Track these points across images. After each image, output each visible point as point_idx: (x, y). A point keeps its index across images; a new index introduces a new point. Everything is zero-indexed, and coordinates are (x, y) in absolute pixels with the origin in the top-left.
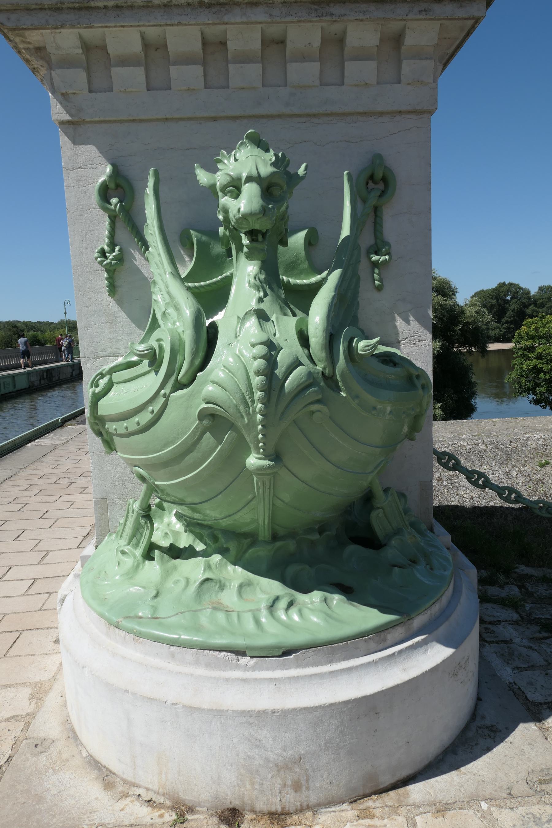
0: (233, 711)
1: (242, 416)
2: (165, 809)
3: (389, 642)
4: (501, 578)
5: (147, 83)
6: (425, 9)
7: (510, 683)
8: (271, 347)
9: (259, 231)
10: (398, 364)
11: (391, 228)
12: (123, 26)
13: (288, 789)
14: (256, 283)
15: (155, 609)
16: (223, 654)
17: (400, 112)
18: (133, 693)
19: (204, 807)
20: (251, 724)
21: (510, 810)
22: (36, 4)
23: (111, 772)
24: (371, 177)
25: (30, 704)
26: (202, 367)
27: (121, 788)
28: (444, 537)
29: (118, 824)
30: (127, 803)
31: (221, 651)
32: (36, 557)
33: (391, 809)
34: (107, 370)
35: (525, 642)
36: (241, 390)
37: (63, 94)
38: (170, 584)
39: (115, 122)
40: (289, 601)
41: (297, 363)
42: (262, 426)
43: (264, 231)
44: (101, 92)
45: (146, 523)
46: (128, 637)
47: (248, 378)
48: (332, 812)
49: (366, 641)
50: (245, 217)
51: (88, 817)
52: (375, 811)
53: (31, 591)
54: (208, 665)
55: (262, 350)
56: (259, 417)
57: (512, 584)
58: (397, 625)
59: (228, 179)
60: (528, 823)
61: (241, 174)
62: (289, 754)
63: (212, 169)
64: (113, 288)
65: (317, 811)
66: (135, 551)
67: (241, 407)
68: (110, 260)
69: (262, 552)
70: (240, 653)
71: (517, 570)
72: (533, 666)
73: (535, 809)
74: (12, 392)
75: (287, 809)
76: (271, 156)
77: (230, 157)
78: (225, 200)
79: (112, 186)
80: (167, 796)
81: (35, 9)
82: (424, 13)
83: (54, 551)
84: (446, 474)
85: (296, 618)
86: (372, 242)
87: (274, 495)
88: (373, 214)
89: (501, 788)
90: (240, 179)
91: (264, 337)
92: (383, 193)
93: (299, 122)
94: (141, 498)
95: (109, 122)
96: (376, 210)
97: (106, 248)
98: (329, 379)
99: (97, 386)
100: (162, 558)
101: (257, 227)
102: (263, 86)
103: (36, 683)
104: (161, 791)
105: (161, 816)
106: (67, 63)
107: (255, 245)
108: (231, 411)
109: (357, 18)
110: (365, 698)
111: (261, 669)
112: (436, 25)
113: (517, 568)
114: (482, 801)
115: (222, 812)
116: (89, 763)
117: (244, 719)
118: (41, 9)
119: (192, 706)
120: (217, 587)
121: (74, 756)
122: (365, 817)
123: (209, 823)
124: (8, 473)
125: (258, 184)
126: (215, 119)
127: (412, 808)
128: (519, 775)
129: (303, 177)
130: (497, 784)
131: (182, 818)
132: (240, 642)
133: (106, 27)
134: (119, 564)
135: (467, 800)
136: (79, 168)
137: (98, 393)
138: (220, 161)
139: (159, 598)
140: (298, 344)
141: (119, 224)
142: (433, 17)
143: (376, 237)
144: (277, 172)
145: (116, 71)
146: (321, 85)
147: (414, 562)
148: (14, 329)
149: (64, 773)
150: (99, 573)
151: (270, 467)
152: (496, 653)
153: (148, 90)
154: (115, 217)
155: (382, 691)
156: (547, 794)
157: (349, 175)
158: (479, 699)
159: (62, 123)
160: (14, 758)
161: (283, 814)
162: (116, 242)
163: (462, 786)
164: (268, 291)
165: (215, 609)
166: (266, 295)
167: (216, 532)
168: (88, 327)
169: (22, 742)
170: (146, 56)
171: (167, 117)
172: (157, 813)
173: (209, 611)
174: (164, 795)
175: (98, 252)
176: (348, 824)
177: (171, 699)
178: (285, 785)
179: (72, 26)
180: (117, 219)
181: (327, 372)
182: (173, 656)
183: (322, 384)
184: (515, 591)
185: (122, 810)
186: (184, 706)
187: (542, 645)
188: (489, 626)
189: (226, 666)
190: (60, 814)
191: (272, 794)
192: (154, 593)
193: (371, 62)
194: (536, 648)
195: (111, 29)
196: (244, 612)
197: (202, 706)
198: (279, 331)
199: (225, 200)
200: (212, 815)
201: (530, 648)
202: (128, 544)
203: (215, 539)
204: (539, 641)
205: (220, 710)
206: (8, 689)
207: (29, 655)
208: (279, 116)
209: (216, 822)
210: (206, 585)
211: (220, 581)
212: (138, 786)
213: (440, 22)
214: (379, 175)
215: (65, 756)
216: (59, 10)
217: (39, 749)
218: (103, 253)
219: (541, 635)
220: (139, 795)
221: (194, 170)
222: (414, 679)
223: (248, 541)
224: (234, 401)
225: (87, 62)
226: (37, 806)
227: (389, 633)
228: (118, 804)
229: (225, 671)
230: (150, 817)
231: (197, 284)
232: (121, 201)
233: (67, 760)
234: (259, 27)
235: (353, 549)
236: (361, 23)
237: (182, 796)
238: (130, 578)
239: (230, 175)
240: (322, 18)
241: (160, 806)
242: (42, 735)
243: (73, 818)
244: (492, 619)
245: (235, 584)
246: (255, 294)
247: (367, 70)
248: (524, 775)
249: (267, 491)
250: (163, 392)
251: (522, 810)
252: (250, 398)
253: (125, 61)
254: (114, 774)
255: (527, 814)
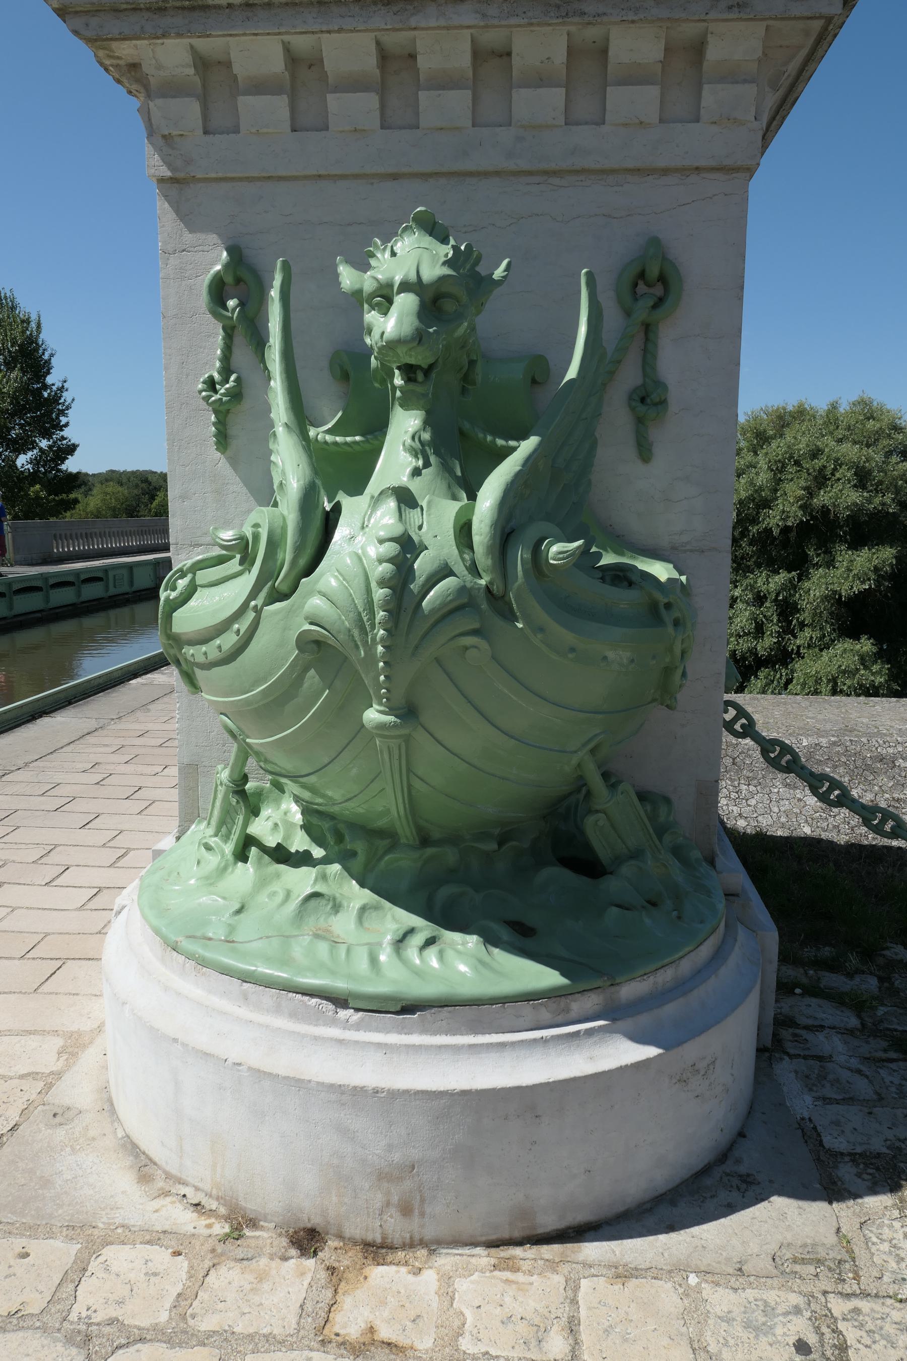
0: (318, 1083)
1: (357, 647)
2: (216, 1219)
3: (573, 1015)
4: (853, 960)
5: (293, 118)
6: (738, 4)
7: (803, 1119)
8: (407, 547)
9: (418, 367)
10: (635, 584)
11: (671, 362)
12: (256, 35)
13: (392, 1210)
14: (413, 444)
15: (232, 929)
16: (314, 1001)
17: (697, 168)
18: (184, 1045)
19: (271, 1222)
20: (343, 1104)
21: (731, 1291)
22: (127, 3)
23: (151, 1160)
24: (642, 275)
25: (58, 1060)
26: (309, 570)
27: (160, 1184)
28: (736, 875)
29: (146, 1228)
30: (165, 1203)
31: (312, 995)
32: (110, 856)
33: (547, 1263)
34: (188, 565)
35: (854, 1063)
36: (356, 607)
37: (164, 137)
38: (263, 898)
39: (240, 179)
40: (429, 936)
41: (445, 571)
42: (384, 663)
43: (425, 366)
44: (222, 133)
45: (238, 802)
46: (187, 965)
47: (369, 591)
48: (457, 1254)
49: (534, 1007)
50: (392, 345)
51: (107, 1214)
52: (522, 1262)
53: (91, 905)
54: (293, 1015)
55: (391, 549)
56: (380, 649)
57: (871, 973)
58: (591, 990)
59: (375, 284)
60: (754, 1312)
61: (393, 278)
62: (397, 1157)
63: (363, 265)
64: (223, 439)
65: (434, 1250)
66: (224, 847)
67: (356, 633)
68: (221, 394)
69: (405, 861)
70: (340, 1001)
71: (887, 953)
72: (851, 1099)
73: (772, 1296)
74: (127, 594)
75: (390, 1241)
76: (447, 251)
77: (384, 249)
78: (371, 317)
79: (229, 280)
80: (222, 1201)
81: (126, 10)
82: (736, 9)
83: (137, 849)
84: (887, 796)
85: (434, 963)
86: (639, 381)
87: (409, 770)
88: (642, 334)
89: (728, 1260)
90: (390, 285)
91: (398, 530)
92: (659, 302)
93: (527, 184)
94: (230, 764)
95: (232, 179)
96: (648, 329)
97: (216, 376)
98: (497, 600)
99: (174, 589)
100: (260, 860)
101: (412, 361)
102: (473, 126)
103: (72, 1033)
104: (214, 1192)
105: (209, 1226)
106: (172, 89)
107: (412, 386)
108: (341, 637)
109: (624, 18)
110: (519, 1089)
111: (369, 1029)
112: (760, 29)
113: (887, 948)
114: (691, 1272)
115: (295, 1232)
116: (124, 1146)
117: (333, 1097)
118: (134, 9)
119: (261, 1069)
120: (329, 907)
121: (105, 1135)
122: (504, 1269)
123: (275, 1244)
124: (92, 724)
125: (417, 294)
126: (395, 177)
127: (579, 1267)
128: (765, 1247)
129: (499, 283)
130: (724, 1254)
131: (237, 1233)
132: (340, 984)
133: (231, 35)
134: (199, 863)
135: (669, 1268)
136: (184, 251)
137: (176, 598)
138: (372, 255)
139: (242, 915)
140: (454, 543)
141: (240, 340)
142: (752, 16)
143: (645, 375)
144: (449, 276)
145: (246, 102)
146: (566, 124)
147: (654, 904)
148: (144, 485)
149: (87, 1155)
150: (169, 874)
151: (395, 726)
152: (796, 1072)
153: (294, 130)
154: (233, 328)
155: (548, 1084)
156: (800, 1278)
157: (589, 275)
158: (741, 1134)
159: (161, 181)
160: (21, 1127)
161: (383, 1247)
162: (232, 368)
163: (668, 1248)
164: (433, 459)
165: (317, 936)
166: (427, 464)
167: (341, 826)
168: (184, 497)
169: (36, 1108)
170: (293, 77)
171: (321, 173)
172: (204, 1221)
173: (307, 939)
174: (218, 1199)
175: (204, 382)
176: (477, 1273)
177: (234, 1057)
178: (388, 1204)
179: (179, 35)
180: (236, 332)
181: (496, 589)
182: (245, 997)
183: (484, 606)
184: (872, 983)
185: (156, 1211)
186: (250, 1069)
187: (881, 1071)
188: (803, 1033)
189: (316, 1018)
190: (69, 1205)
191: (368, 1214)
192: (237, 906)
193: (651, 87)
194: (868, 1073)
195: (237, 38)
196: (357, 945)
197: (275, 1071)
198: (428, 522)
199: (371, 317)
200: (280, 1235)
201: (859, 1072)
202: (216, 835)
203: (340, 838)
204: (877, 1064)
205: (299, 1080)
206: (32, 1036)
207: (70, 994)
208: (497, 173)
209: (285, 1244)
210: (313, 903)
211: (334, 899)
212: (185, 1184)
213: (765, 23)
214: (653, 272)
215: (91, 1133)
216: (161, 10)
217: (58, 1119)
218: (211, 384)
219: (884, 1055)
220: (184, 1196)
221: (335, 267)
222: (603, 1073)
223: (386, 842)
224: (347, 623)
225: (204, 86)
226: (40, 1191)
227: (575, 1001)
228: (152, 1203)
229: (316, 1025)
230: (193, 1225)
231: (349, 439)
232: (242, 304)
233: (94, 1139)
234: (467, 33)
235: (556, 875)
236: (631, 25)
237: (243, 1203)
238: (211, 884)
239: (376, 279)
240: (566, 19)
241: (212, 1213)
242: (67, 1102)
243: (87, 1213)
244: (810, 1022)
245: (356, 905)
246: (411, 462)
247: (644, 100)
248: (773, 1247)
249: (396, 763)
250: (253, 603)
251: (750, 1294)
252: (369, 620)
253: (260, 87)
254: (155, 1164)
255: (756, 1300)
